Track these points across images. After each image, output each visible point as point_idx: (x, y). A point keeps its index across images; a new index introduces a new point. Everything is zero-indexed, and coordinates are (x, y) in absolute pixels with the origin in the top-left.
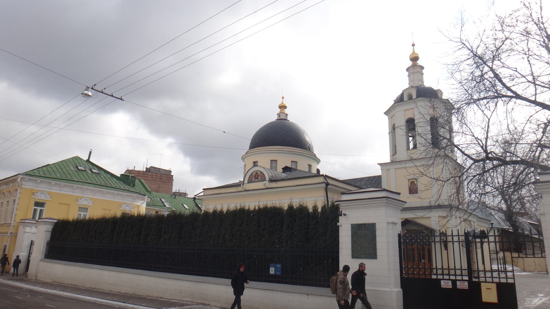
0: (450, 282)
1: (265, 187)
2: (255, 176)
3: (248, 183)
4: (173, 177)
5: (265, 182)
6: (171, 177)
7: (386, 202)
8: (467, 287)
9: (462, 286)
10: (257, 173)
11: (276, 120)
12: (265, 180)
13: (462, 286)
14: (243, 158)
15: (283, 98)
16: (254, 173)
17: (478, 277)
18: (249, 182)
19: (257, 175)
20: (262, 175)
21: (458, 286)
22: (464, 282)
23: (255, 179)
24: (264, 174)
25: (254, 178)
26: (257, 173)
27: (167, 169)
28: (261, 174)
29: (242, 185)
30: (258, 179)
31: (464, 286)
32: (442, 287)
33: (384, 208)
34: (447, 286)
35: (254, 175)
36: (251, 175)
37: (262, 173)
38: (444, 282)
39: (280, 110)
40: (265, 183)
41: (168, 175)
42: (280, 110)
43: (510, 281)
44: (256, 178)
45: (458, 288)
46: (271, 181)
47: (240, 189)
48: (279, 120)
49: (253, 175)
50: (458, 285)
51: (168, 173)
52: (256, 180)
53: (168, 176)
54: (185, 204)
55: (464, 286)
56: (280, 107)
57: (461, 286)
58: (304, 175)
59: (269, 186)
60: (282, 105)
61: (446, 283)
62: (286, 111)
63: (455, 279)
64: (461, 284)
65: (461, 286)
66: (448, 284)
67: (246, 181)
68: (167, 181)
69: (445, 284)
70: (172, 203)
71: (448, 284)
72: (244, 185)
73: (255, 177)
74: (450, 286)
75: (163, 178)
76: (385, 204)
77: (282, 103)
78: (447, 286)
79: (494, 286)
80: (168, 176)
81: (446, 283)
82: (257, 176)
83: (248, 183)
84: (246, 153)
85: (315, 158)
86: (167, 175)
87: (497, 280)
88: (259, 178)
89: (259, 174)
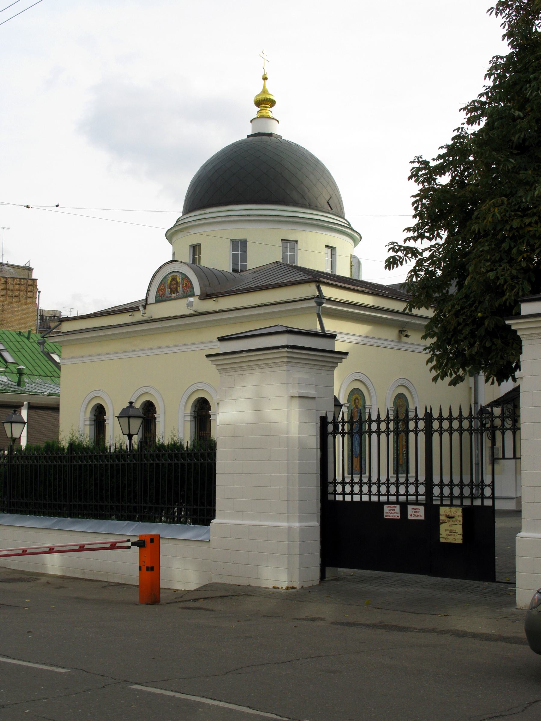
0: (398, 507)
1: (191, 312)
2: (171, 284)
3: (157, 301)
4: (38, 284)
5: (191, 299)
6: (30, 283)
7: (288, 357)
8: (399, 515)
9: (391, 513)
10: (174, 279)
11: (249, 136)
12: (193, 295)
13: (391, 513)
14: (171, 235)
15: (265, 79)
16: (169, 279)
17: (335, 493)
18: (158, 301)
19: (174, 282)
20: (185, 282)
21: (385, 514)
22: (395, 507)
23: (171, 294)
24: (190, 282)
25: (168, 291)
26: (174, 279)
27: (22, 264)
28: (183, 279)
29: (141, 308)
30: (178, 292)
31: (394, 513)
32: (410, 518)
33: (285, 368)
34: (417, 516)
35: (169, 283)
36: (162, 283)
37: (185, 277)
38: (412, 509)
39: (259, 109)
40: (191, 303)
41: (24, 279)
42: (259, 109)
43: (488, 503)
44: (174, 290)
45: (385, 517)
46: (205, 296)
47: (138, 316)
48: (257, 138)
49: (165, 283)
50: (411, 515)
51: (25, 275)
52: (174, 295)
53: (23, 282)
54: (55, 353)
55: (394, 513)
56: (258, 103)
57: (389, 515)
58: (133, 306)
59: (201, 309)
60: (263, 97)
61: (415, 511)
62: (273, 112)
63: (342, 500)
64: (389, 510)
65: (389, 515)
66: (418, 512)
67: (152, 299)
68: (22, 294)
69: (415, 512)
70: (22, 350)
71: (418, 512)
72: (147, 307)
73: (171, 289)
74: (421, 516)
75: (11, 287)
76: (286, 359)
77: (264, 91)
78: (417, 516)
79: (458, 512)
80: (23, 282)
81: (415, 511)
82: (175, 286)
83: (157, 301)
84: (177, 222)
85: (349, 231)
86: (20, 279)
87: (467, 502)
88: (180, 289)
89: (179, 280)
